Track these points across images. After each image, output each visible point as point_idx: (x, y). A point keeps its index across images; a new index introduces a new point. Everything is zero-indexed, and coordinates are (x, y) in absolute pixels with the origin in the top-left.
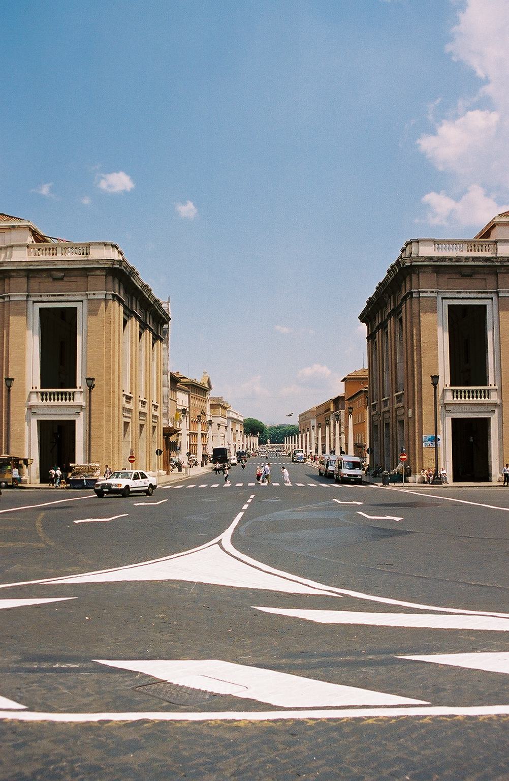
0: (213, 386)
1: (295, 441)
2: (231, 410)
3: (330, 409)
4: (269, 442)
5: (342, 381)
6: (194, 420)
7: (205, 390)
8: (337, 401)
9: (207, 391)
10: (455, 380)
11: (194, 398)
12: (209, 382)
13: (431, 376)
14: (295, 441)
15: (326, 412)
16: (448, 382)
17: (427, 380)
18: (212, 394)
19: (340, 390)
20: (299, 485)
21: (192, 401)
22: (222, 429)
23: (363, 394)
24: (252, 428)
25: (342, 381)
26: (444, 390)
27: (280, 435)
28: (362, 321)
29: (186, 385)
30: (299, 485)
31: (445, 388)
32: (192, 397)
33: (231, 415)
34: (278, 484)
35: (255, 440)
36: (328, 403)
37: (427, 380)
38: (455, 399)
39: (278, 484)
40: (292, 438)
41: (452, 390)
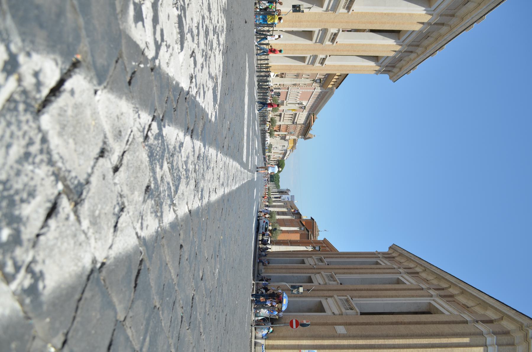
8: (298, 214)
12: (309, 138)
18: (301, 141)
19: (305, 216)
21: (300, 126)
23: (307, 232)
29: (309, 123)
33: (288, 152)
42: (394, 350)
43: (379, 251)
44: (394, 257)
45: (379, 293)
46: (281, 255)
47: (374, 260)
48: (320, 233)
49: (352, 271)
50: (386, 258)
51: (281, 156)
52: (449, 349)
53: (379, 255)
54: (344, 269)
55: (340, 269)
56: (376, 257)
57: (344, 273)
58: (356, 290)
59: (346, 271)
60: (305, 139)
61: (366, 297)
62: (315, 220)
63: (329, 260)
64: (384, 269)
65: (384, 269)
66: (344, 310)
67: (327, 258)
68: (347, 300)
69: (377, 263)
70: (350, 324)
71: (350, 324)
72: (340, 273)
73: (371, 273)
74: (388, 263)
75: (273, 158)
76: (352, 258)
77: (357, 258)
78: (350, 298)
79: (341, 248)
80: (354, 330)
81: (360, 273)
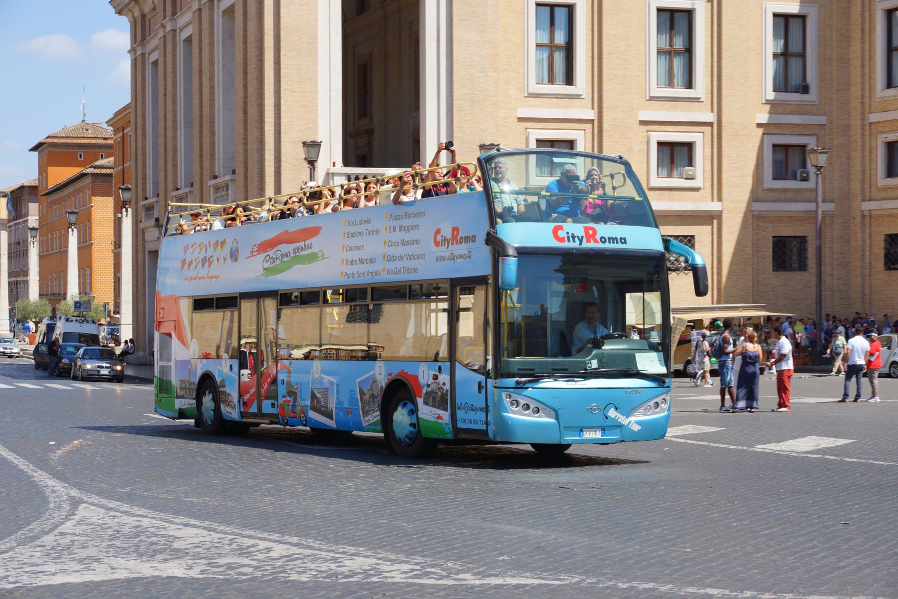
5: (34, 149)
23: (88, 181)
25: (34, 149)
28: (119, 13)
31: (333, 170)
43: (129, 48)
44: (143, 16)
46: (141, 306)
47: (149, 69)
48: (89, 120)
49: (170, 146)
50: (144, 38)
52: (283, 33)
53: (139, 53)
56: (143, 63)
58: (201, 156)
59: (170, 160)
61: (213, 144)
62: (41, 139)
63: (150, 187)
67: (144, 189)
68: (217, 188)
72: (175, 176)
74: (154, 42)
76: (144, 125)
77: (144, 112)
78: (213, 182)
79: (125, 98)
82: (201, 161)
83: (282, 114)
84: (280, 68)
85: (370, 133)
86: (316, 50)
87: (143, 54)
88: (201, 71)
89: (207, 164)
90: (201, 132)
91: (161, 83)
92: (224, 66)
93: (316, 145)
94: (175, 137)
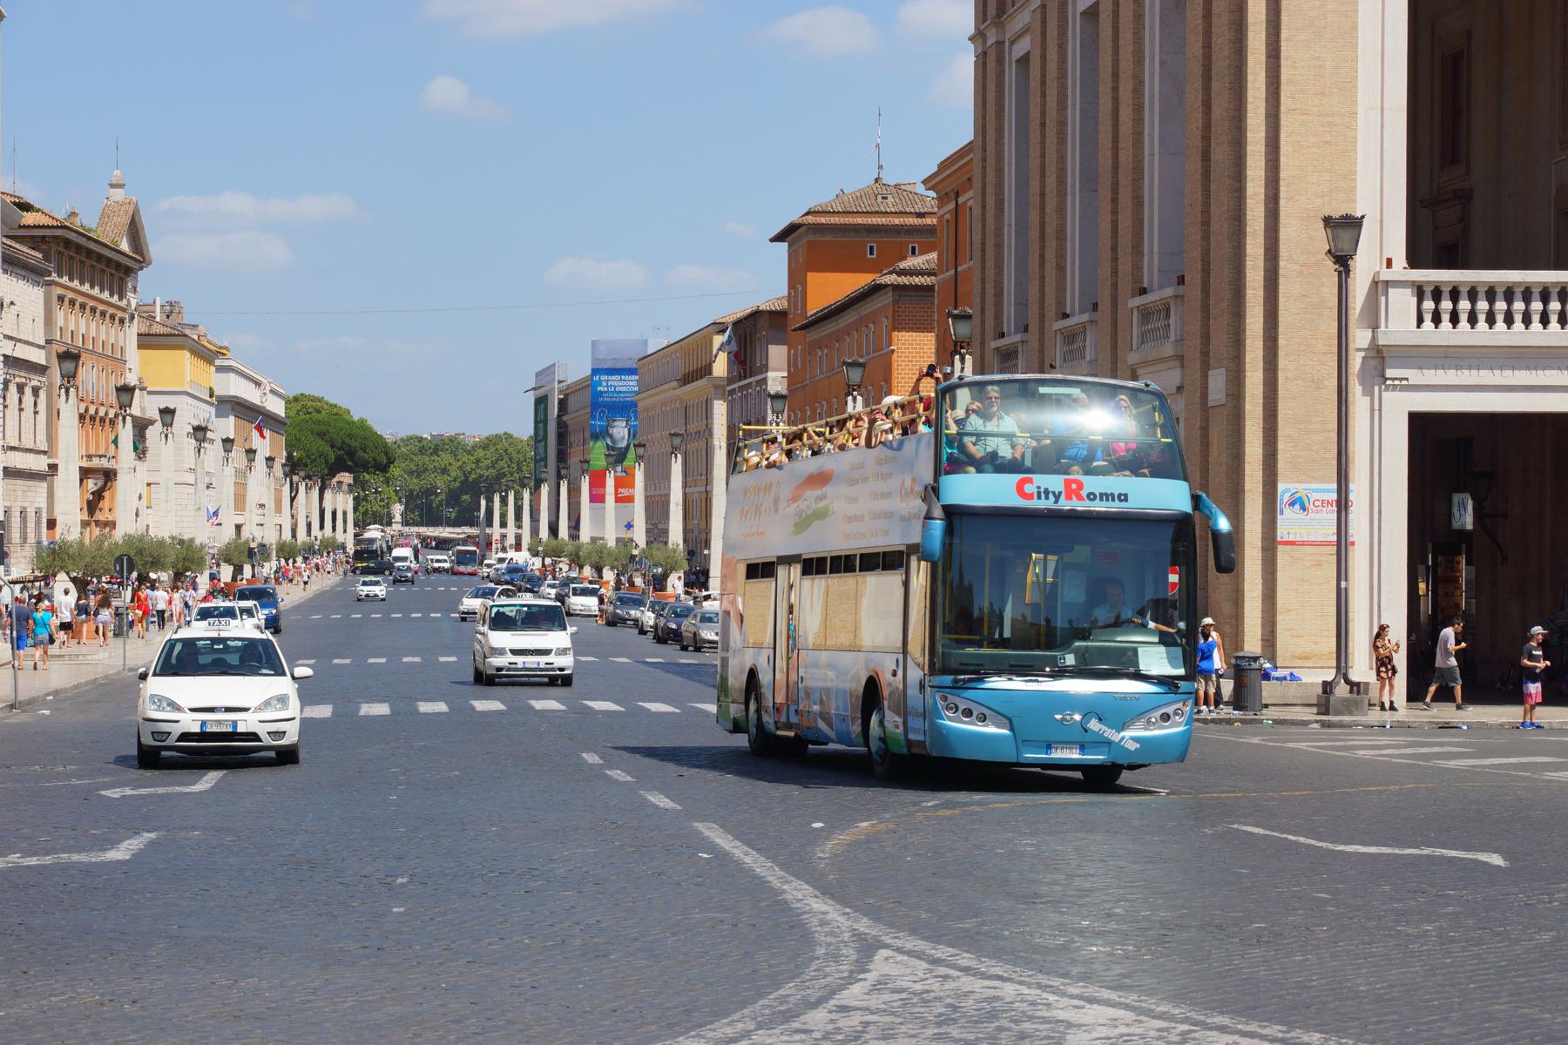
0: (154, 248)
1: (518, 517)
2: (232, 363)
3: (706, 370)
4: (398, 518)
5: (779, 238)
6: (102, 414)
7: (118, 265)
8: (749, 334)
9: (128, 271)
10: (1440, 232)
11: (83, 306)
12: (135, 231)
13: (1328, 221)
14: (518, 517)
15: (686, 379)
16: (1397, 246)
17: (1303, 242)
18: (148, 288)
19: (764, 281)
20: (599, 705)
22: (214, 450)
23: (885, 299)
24: (326, 447)
25: (779, 238)
26: (1375, 283)
27: (455, 488)
30: (599, 705)
31: (1386, 275)
32: (61, 299)
34: (442, 707)
35: (341, 501)
36: (696, 345)
37: (1303, 242)
38: (1428, 324)
39: (442, 707)
40: (504, 501)
41: (1413, 283)
42: (1282, 202)
43: (971, 30)
45: (1125, 157)
48: (889, 178)
49: (1051, 230)
51: (264, 445)
54: (1042, 256)
55: (1042, 278)
56: (1000, 60)
57: (1061, 268)
59: (1050, 256)
60: (140, 257)
62: (794, 216)
64: (1044, 46)
65: (1044, 46)
66: (1168, 349)
68: (1146, 314)
69: (1024, 61)
70: (1205, 354)
71: (1205, 354)
72: (1061, 289)
73: (1061, 137)
75: (278, 509)
80: (1219, 340)
81: (1062, 194)
82: (1115, 260)
83: (1283, 160)
84: (1278, 66)
85: (1464, 197)
86: (1355, 28)
87: (1000, 43)
88: (1116, 76)
89: (1125, 266)
90: (1115, 200)
91: (1035, 101)
92: (1162, 63)
93: (1352, 224)
94: (1061, 211)
